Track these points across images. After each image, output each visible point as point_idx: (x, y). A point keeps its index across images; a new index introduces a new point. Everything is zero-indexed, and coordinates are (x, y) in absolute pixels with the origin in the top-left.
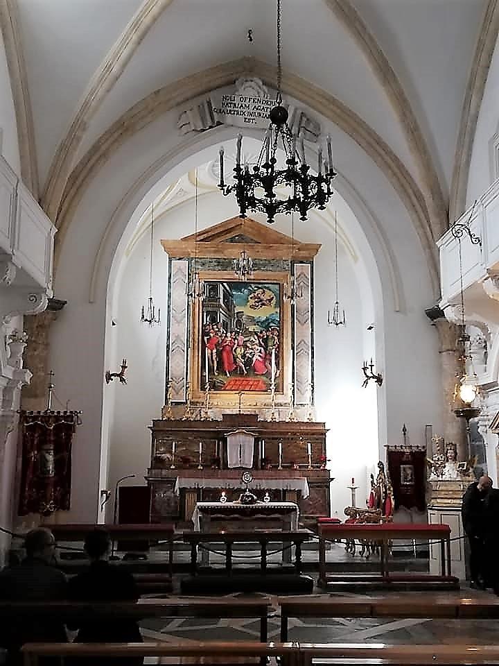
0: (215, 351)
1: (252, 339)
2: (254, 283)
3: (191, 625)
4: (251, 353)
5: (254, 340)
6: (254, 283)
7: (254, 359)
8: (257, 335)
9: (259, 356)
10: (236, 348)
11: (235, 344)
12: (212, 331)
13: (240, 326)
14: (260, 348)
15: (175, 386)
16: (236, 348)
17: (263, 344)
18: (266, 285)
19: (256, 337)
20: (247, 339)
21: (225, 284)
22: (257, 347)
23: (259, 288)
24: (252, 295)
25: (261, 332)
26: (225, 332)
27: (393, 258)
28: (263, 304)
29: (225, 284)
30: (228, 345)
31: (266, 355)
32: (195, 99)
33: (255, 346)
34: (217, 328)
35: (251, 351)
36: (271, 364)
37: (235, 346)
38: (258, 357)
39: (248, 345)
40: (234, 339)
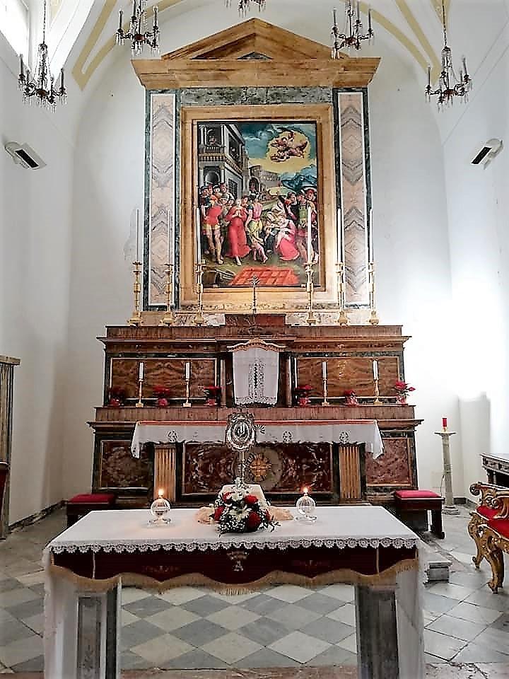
0: (217, 227)
1: (275, 207)
7: (279, 238)
8: (283, 201)
9: (287, 233)
11: (248, 215)
23: (284, 130)
24: (274, 141)
25: (289, 197)
26: (233, 198)
28: (292, 154)
30: (238, 217)
36: (305, 244)
37: (250, 219)
39: (270, 216)
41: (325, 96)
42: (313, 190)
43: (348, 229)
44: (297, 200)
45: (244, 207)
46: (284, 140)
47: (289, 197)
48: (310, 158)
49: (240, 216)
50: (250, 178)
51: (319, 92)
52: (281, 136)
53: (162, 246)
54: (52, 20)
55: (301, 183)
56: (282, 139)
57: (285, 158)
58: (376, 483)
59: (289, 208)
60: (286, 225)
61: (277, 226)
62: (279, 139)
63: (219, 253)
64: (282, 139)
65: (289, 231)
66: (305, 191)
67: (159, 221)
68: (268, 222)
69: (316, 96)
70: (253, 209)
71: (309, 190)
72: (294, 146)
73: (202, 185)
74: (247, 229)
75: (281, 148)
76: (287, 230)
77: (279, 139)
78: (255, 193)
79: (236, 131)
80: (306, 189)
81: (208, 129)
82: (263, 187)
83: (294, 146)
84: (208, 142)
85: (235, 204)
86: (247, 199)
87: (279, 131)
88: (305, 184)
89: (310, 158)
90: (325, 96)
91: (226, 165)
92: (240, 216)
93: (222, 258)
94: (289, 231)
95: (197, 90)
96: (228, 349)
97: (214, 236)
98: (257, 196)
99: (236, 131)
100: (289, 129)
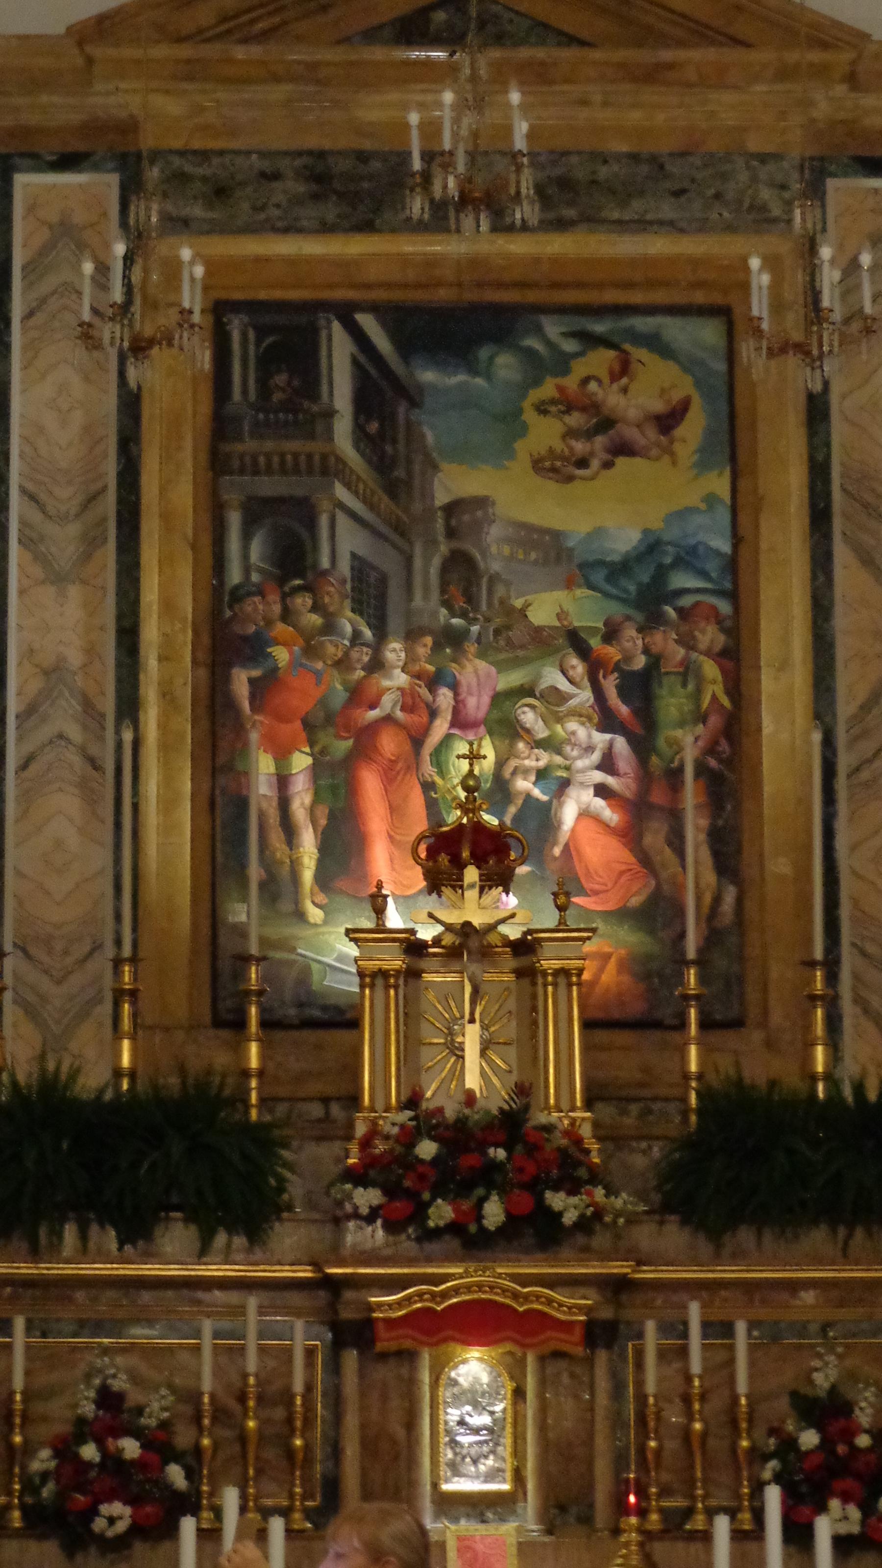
0: (301, 761)
1: (553, 678)
2: (561, 310)
3: (134, 1343)
4: (542, 775)
5: (563, 684)
6: (561, 310)
7: (569, 814)
8: (583, 651)
9: (601, 790)
10: (447, 740)
11: (433, 713)
12: (281, 629)
13: (471, 599)
14: (601, 739)
15: (43, 999)
16: (447, 740)
17: (624, 710)
18: (642, 324)
19: (578, 667)
20: (514, 679)
21: (367, 321)
22: (581, 731)
23: (591, 340)
24: (548, 389)
25: (611, 634)
26: (368, 633)
27: (661, 223)
28: (623, 449)
29: (367, 321)
30: (388, 719)
31: (645, 776)
32: (96, 954)
33: (573, 725)
34: (316, 608)
35: (544, 758)
36: (676, 841)
37: (441, 727)
38: (587, 796)
39: (529, 717)
40: (433, 682)
41: (766, 194)
42: (714, 608)
43: (865, 775)
44: (646, 651)
45: (418, 676)
46: (593, 386)
47: (611, 634)
48: (703, 465)
49: (399, 714)
50: (444, 548)
51: (743, 177)
52: (580, 369)
53: (59, 844)
54: (551, 1287)
55: (661, 574)
56: (585, 381)
57: (595, 464)
58: (489, 1276)
59: (610, 685)
60: (596, 757)
61: (558, 759)
62: (571, 382)
63: (308, 876)
64: (585, 381)
65: (610, 780)
66: (683, 613)
67: (46, 732)
68: (521, 745)
69: (730, 195)
70: (455, 687)
71: (697, 604)
72: (633, 414)
73: (235, 576)
74: (429, 770)
75: (575, 419)
76: (599, 777)
77: (571, 382)
78: (464, 615)
79: (382, 342)
80: (686, 601)
81: (262, 332)
82: (500, 591)
83: (633, 414)
84: (264, 390)
85: (377, 665)
86: (429, 640)
87: (570, 346)
88: (681, 580)
89: (703, 465)
90: (766, 194)
91: (341, 492)
92: (399, 714)
93: (321, 898)
94: (610, 780)
95: (216, 161)
96: (371, 1308)
97: (284, 804)
98: (475, 629)
99: (382, 342)
100: (616, 339)
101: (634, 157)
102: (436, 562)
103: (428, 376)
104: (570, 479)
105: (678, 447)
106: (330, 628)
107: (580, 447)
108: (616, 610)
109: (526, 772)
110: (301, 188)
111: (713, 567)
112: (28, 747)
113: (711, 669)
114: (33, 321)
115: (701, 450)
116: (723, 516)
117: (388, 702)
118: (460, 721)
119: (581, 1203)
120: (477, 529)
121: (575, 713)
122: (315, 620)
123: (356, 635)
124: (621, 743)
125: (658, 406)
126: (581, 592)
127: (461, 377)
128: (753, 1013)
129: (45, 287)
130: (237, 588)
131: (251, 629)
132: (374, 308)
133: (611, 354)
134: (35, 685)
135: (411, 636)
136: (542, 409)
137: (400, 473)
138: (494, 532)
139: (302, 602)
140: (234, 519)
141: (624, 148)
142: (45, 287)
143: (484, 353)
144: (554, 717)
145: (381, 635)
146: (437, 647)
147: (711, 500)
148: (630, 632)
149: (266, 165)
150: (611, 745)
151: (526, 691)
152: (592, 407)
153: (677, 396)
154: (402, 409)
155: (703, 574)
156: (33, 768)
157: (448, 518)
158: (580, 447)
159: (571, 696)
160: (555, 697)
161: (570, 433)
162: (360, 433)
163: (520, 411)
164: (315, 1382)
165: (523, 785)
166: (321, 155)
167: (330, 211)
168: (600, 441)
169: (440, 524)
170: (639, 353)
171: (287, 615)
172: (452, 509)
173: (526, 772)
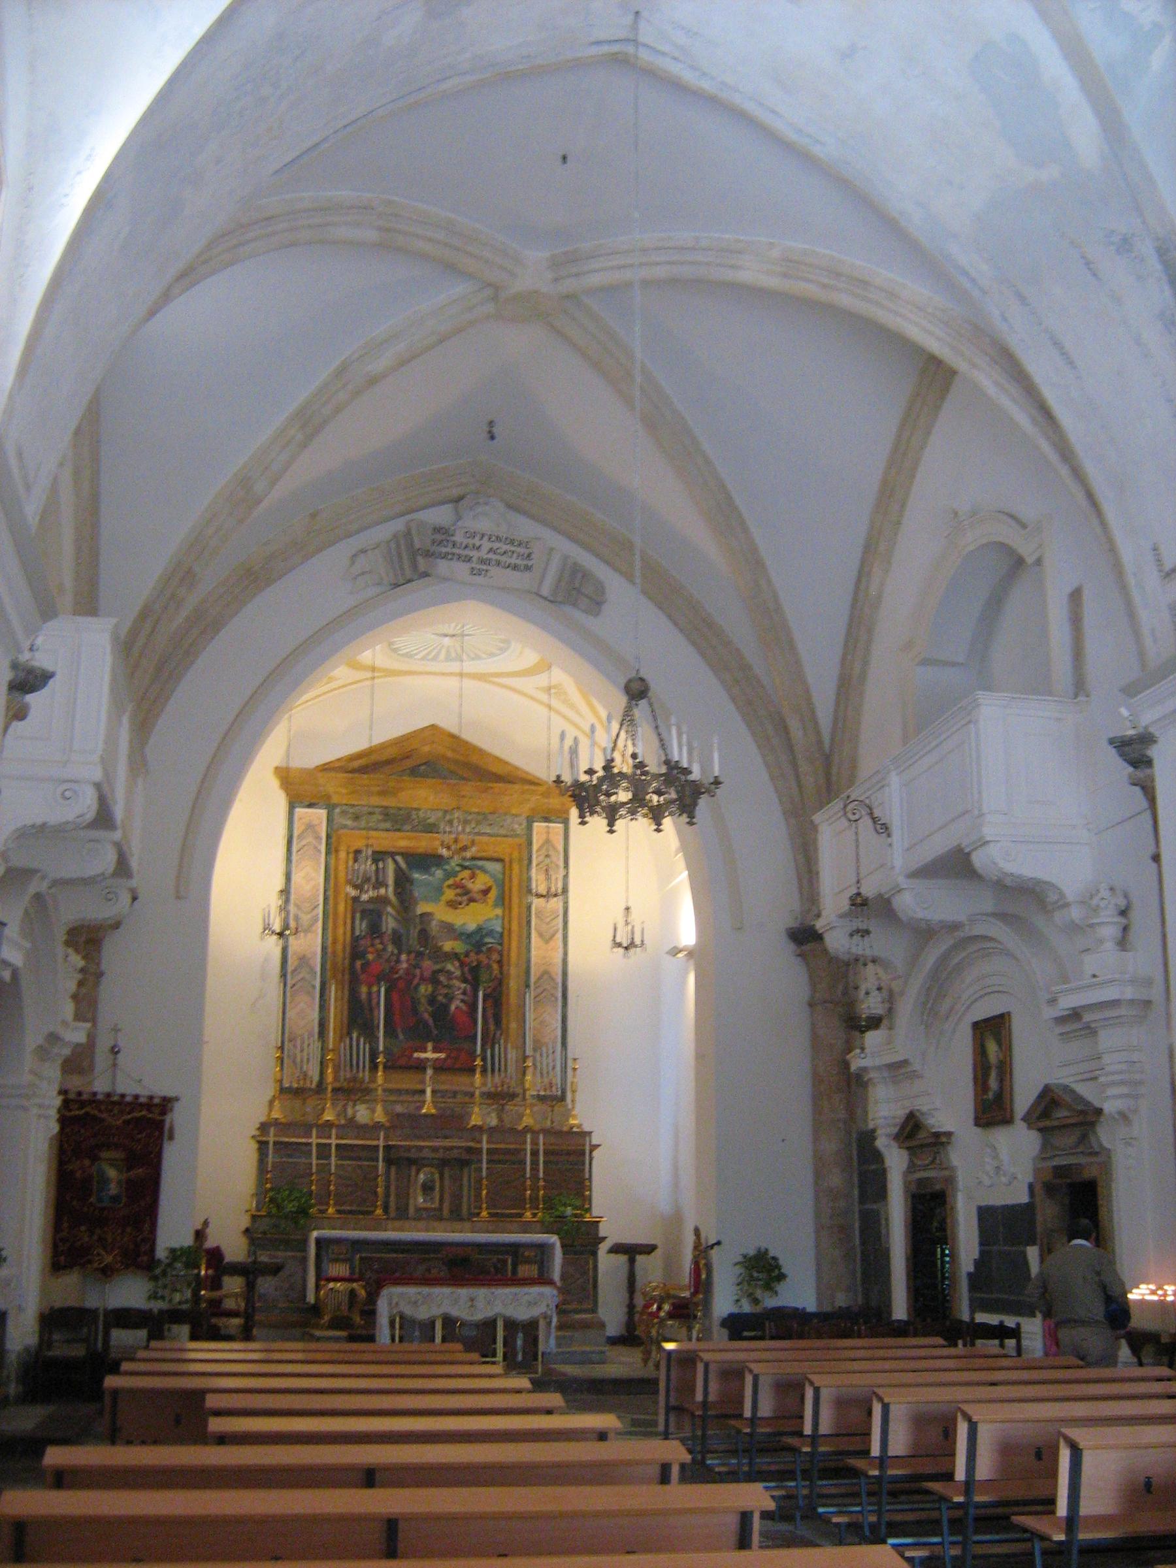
1: (449, 967)
4: (446, 995)
5: (452, 969)
7: (453, 1007)
8: (459, 959)
9: (462, 1001)
11: (414, 976)
14: (463, 985)
18: (480, 863)
19: (457, 964)
20: (438, 967)
21: (399, 858)
22: (456, 983)
23: (466, 868)
24: (451, 882)
28: (472, 900)
30: (400, 978)
34: (382, 943)
37: (416, 981)
39: (442, 978)
50: (419, 928)
52: (461, 876)
56: (462, 879)
59: (466, 969)
64: (462, 879)
73: (357, 933)
75: (458, 891)
76: (461, 997)
77: (458, 879)
85: (398, 961)
87: (458, 869)
89: (496, 906)
91: (389, 909)
101: (478, 813)
102: (417, 931)
103: (416, 876)
104: (456, 908)
105: (489, 900)
106: (384, 949)
107: (459, 899)
108: (468, 947)
109: (441, 994)
110: (380, 818)
111: (497, 936)
112: (293, 982)
113: (495, 966)
114: (299, 853)
115: (495, 901)
116: (500, 921)
117: (401, 972)
118: (422, 979)
119: (389, 954)
120: (430, 922)
121: (456, 978)
122: (380, 947)
123: (392, 952)
124: (468, 987)
125: (483, 887)
126: (459, 942)
127: (426, 876)
128: (350, 902)
129: (304, 842)
130: (358, 937)
131: (362, 949)
132: (402, 854)
133: (470, 871)
134: (296, 963)
135: (409, 953)
136: (449, 886)
137: (406, 905)
138: (434, 923)
139: (377, 941)
140: (358, 915)
141: (477, 810)
142: (304, 842)
143: (433, 869)
144: (450, 979)
145: (400, 953)
146: (416, 957)
147: (497, 916)
148: (472, 954)
149: (370, 810)
150: (465, 987)
151: (441, 971)
152: (463, 887)
153: (489, 884)
154: (408, 885)
155: (493, 937)
156: (295, 988)
157: (421, 918)
158: (459, 899)
159: (454, 973)
160: (449, 972)
161: (457, 895)
162: (395, 890)
163: (442, 888)
164: (376, 1022)
165: (440, 998)
166: (386, 807)
167: (388, 825)
168: (465, 898)
169: (417, 921)
170: (478, 872)
171: (373, 945)
172: (421, 915)
173: (441, 994)
